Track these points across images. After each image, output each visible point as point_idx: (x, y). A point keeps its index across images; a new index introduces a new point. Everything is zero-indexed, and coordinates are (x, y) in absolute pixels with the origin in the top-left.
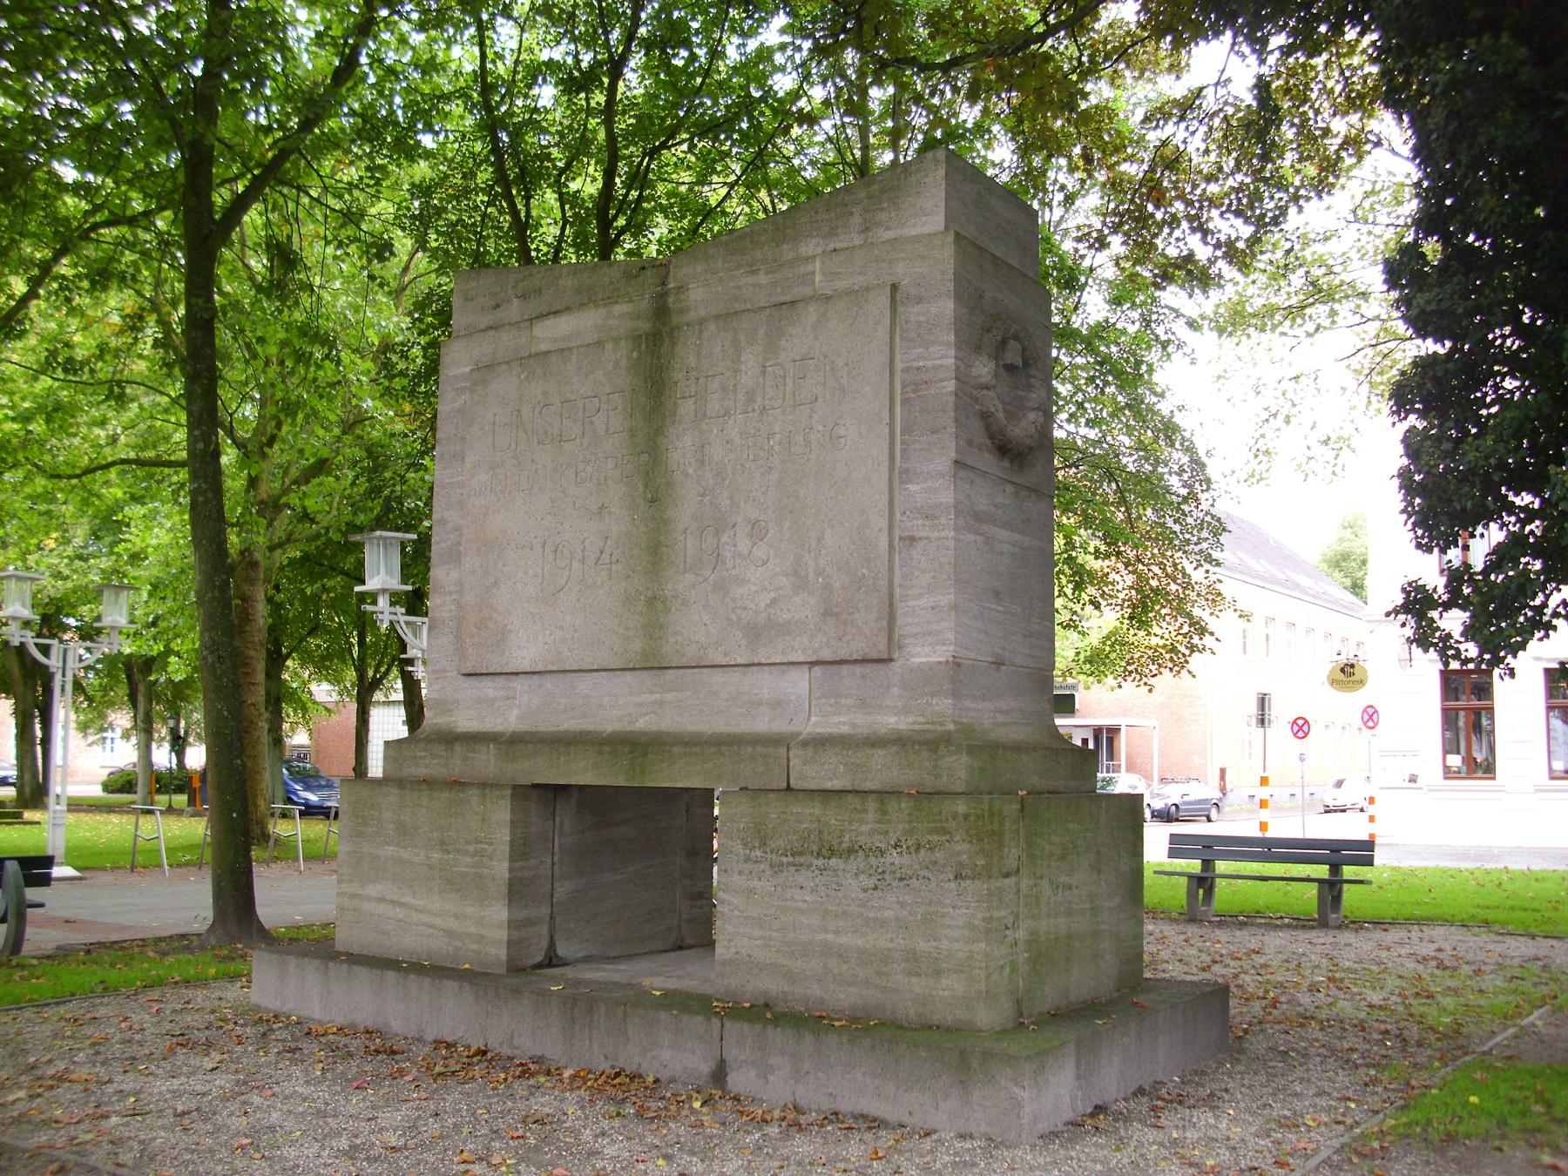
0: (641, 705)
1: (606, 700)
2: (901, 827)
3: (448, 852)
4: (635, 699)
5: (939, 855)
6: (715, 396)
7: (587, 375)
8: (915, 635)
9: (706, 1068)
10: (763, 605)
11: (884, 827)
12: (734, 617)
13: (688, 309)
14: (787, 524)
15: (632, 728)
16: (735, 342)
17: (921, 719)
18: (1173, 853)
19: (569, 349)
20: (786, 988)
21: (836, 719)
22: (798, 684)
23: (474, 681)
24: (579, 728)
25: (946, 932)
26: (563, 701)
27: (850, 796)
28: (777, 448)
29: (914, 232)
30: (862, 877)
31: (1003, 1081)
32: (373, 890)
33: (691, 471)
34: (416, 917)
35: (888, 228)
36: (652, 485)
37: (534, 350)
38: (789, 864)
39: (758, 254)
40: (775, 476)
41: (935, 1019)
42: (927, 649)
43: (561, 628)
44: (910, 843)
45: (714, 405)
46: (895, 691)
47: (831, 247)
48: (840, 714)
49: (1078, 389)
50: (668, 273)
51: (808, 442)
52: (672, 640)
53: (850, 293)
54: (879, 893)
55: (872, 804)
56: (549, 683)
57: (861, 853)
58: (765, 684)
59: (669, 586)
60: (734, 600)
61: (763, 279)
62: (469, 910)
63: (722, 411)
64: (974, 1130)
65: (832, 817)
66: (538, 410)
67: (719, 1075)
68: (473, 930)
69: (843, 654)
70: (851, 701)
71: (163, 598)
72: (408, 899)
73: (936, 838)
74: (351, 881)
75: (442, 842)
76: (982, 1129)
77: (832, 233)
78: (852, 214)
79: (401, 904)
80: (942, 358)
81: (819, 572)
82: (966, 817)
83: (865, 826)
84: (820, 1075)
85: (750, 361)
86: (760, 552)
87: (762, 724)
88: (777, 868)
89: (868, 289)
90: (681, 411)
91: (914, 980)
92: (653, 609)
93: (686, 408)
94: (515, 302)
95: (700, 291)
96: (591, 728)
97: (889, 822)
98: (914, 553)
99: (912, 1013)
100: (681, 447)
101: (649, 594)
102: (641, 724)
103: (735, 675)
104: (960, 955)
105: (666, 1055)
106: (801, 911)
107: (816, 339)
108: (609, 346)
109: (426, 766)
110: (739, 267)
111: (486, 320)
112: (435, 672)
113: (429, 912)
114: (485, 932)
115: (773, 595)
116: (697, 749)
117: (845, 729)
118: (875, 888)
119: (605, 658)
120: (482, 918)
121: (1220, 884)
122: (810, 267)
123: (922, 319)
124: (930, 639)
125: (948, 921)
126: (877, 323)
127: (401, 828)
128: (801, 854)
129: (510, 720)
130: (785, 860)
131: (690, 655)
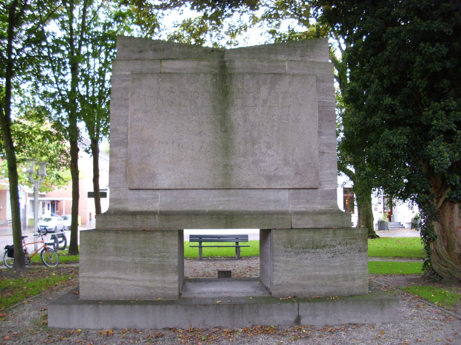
0: (220, 201)
1: (203, 199)
2: (341, 238)
3: (145, 257)
4: (217, 199)
5: (353, 246)
8: (325, 181)
9: (292, 319)
10: (272, 170)
11: (335, 239)
12: (261, 173)
13: (235, 69)
14: (281, 144)
15: (217, 209)
16: (258, 82)
17: (328, 206)
18: (191, 241)
19: (183, 74)
20: (302, 291)
21: (299, 206)
22: (285, 195)
24: (193, 209)
25: (357, 268)
27: (323, 230)
28: (276, 120)
30: (328, 254)
31: (393, 306)
32: (102, 274)
33: (241, 123)
34: (127, 283)
35: (310, 58)
36: (224, 126)
37: (162, 71)
38: (302, 252)
39: (262, 56)
41: (353, 293)
42: (329, 186)
43: (183, 173)
44: (344, 243)
45: (250, 102)
46: (319, 198)
47: (290, 59)
48: (300, 205)
52: (235, 179)
53: (303, 75)
54: (334, 258)
55: (331, 232)
56: (175, 193)
57: (327, 247)
58: (272, 195)
59: (233, 161)
60: (260, 167)
61: (265, 64)
62: (157, 278)
64: (385, 321)
65: (317, 236)
67: (298, 321)
68: (160, 285)
69: (303, 186)
70: (304, 201)
72: (124, 276)
73: (352, 241)
74: (88, 271)
75: (141, 254)
76: (388, 321)
77: (290, 55)
78: (297, 50)
79: (118, 279)
80: (331, 100)
82: (362, 234)
83: (329, 238)
84: (335, 314)
85: (264, 91)
86: (271, 152)
87: (272, 208)
88: (297, 254)
89: (308, 75)
91: (346, 283)
92: (227, 169)
93: (238, 102)
95: (240, 63)
96: (198, 209)
97: (337, 237)
99: (346, 292)
100: (236, 115)
101: (224, 163)
103: (260, 192)
104: (361, 274)
105: (276, 318)
106: (307, 266)
107: (289, 87)
109: (121, 224)
112: (114, 188)
113: (135, 280)
114: (167, 285)
115: (276, 166)
118: (333, 257)
119: (204, 184)
120: (164, 281)
121: (241, 249)
122: (284, 64)
123: (325, 87)
124: (330, 183)
125: (357, 264)
126: (312, 86)
127: (117, 249)
128: (306, 248)
129: (157, 206)
130: (300, 251)
131: (243, 184)
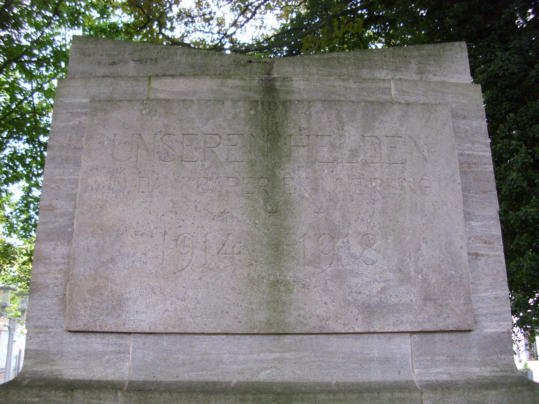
6: (326, 149)
7: (208, 119)
8: (485, 315)
10: (375, 291)
16: (339, 117)
17: (496, 369)
21: (434, 370)
22: (404, 346)
23: (82, 338)
24: (202, 379)
26: (181, 357)
29: (453, 80)
33: (307, 195)
35: (435, 75)
36: (273, 201)
37: (151, 96)
40: (378, 206)
42: (494, 324)
43: (183, 299)
45: (324, 153)
46: (475, 351)
47: (398, 77)
48: (436, 367)
49: (366, 186)
50: (272, 68)
51: (402, 188)
52: (295, 313)
56: (165, 342)
58: (375, 347)
59: (291, 274)
60: (350, 287)
63: (331, 159)
66: (158, 137)
70: (444, 358)
71: (124, 303)
80: (484, 151)
81: (419, 271)
85: (352, 133)
90: (295, 154)
92: (278, 290)
93: (301, 153)
94: (132, 64)
98: (479, 263)
100: (296, 179)
101: (272, 278)
102: (263, 376)
103: (349, 341)
108: (228, 104)
110: (330, 75)
111: (101, 71)
115: (383, 285)
116: (341, 396)
117: (445, 377)
122: (386, 85)
123: (468, 128)
124: (496, 317)
126: (445, 124)
131: (313, 324)
